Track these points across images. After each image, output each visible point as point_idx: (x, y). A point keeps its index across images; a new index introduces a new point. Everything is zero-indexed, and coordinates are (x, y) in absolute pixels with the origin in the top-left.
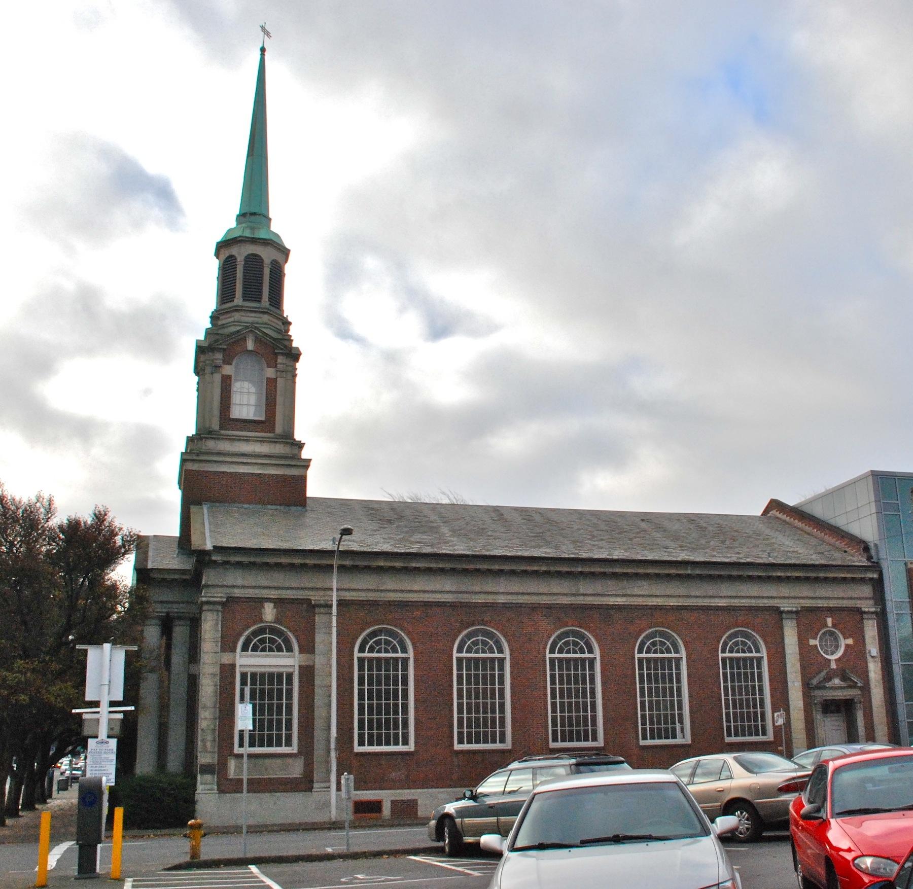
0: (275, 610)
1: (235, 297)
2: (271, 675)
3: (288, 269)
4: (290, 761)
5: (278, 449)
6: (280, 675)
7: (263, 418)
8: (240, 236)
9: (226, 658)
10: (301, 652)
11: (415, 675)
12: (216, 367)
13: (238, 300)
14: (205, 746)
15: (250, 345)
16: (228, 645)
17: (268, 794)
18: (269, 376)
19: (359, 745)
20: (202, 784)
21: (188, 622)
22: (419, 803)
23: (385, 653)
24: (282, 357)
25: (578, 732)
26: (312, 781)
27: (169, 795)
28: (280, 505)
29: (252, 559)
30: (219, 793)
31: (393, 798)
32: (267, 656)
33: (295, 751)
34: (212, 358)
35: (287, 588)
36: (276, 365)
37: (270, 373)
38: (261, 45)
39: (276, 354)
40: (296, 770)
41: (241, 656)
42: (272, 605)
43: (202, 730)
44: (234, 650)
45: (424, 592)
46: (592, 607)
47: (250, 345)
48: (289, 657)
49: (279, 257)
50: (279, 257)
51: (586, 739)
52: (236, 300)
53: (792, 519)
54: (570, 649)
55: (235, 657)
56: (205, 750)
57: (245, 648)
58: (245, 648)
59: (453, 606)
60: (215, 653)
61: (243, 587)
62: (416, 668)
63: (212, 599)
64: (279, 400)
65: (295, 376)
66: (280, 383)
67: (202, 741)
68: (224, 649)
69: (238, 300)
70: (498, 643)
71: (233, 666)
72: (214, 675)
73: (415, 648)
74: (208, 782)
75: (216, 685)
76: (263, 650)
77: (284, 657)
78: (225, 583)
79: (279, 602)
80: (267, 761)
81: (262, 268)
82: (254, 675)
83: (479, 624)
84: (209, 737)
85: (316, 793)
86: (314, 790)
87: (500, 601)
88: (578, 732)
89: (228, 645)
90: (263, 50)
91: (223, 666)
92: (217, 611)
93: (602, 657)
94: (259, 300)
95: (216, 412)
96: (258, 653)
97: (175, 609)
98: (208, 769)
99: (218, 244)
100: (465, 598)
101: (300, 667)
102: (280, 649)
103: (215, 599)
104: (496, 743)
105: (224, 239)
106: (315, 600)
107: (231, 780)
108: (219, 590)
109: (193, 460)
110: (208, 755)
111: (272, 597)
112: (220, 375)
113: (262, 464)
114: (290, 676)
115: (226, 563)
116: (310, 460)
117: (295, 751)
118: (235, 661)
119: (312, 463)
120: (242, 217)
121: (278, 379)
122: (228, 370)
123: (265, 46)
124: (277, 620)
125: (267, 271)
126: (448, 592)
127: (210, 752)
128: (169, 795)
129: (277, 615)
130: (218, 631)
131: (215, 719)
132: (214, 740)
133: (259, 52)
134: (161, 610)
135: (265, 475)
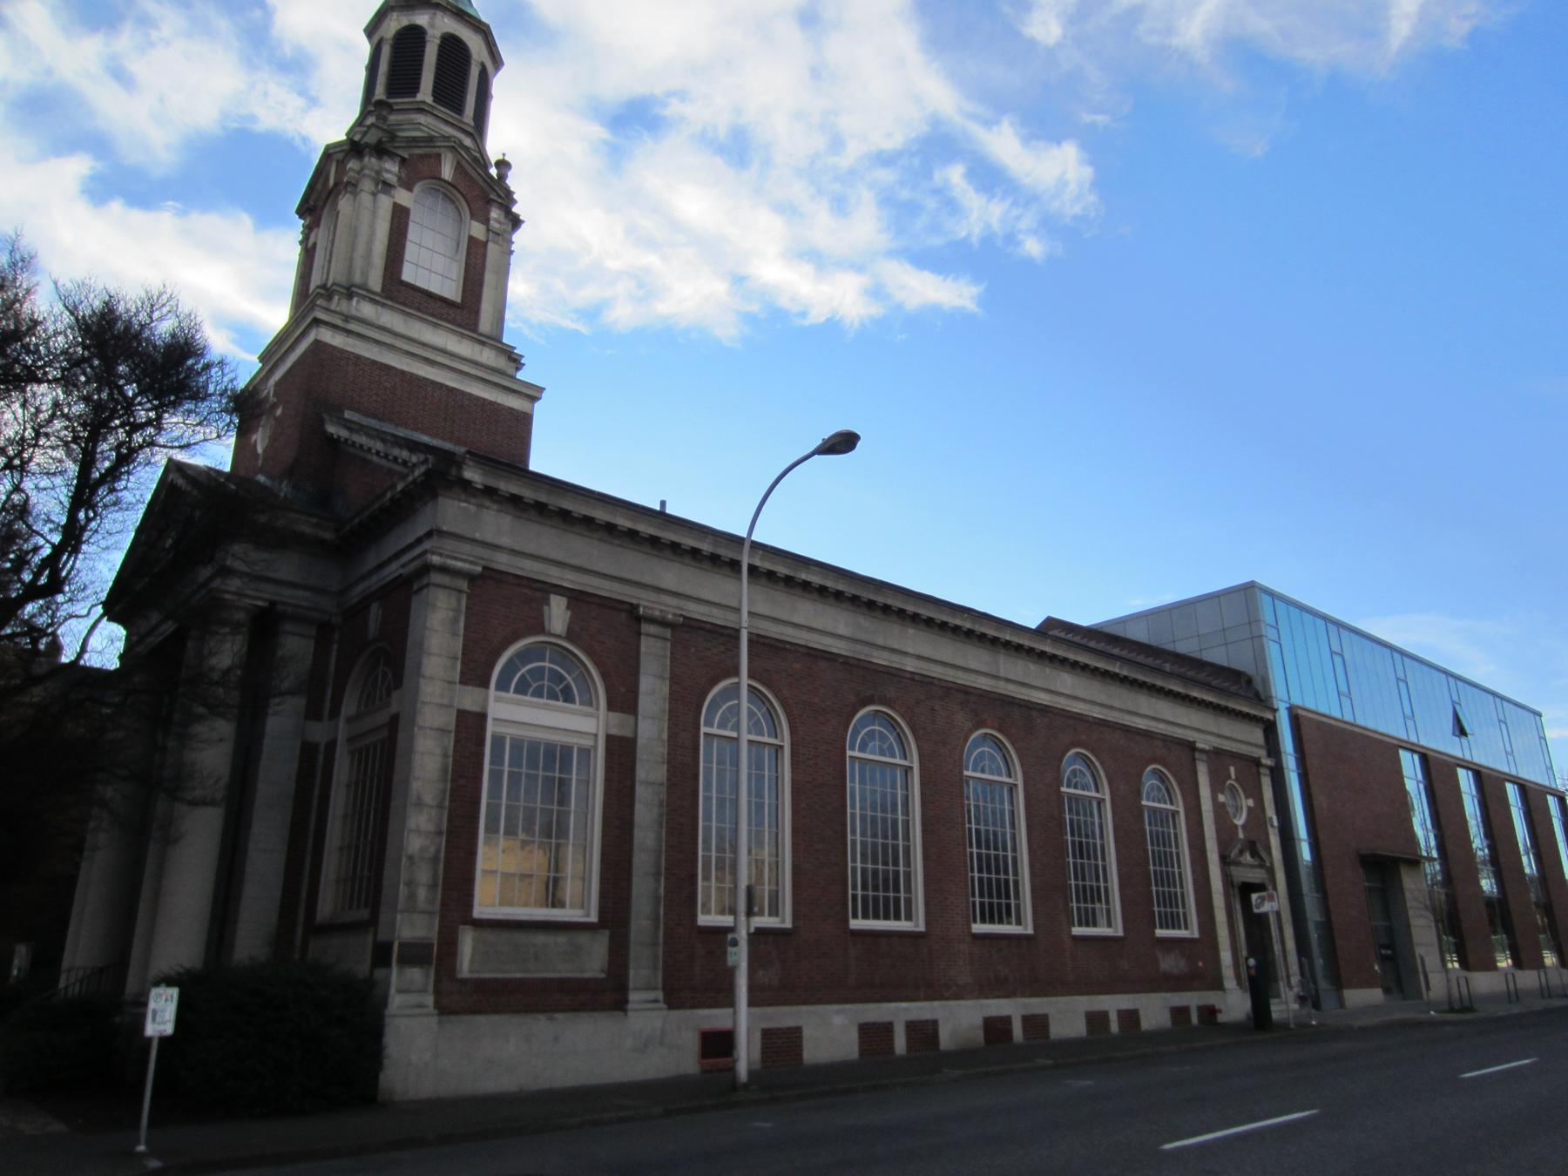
2: (550, 749)
4: (583, 938)
5: (487, 356)
6: (566, 750)
9: (468, 699)
10: (612, 706)
13: (425, 93)
14: (412, 897)
16: (475, 672)
17: (542, 1018)
20: (400, 991)
21: (313, 632)
24: (498, 212)
31: (765, 1026)
32: (546, 707)
33: (594, 918)
35: (699, 601)
37: (477, 230)
39: (489, 202)
40: (593, 960)
41: (497, 700)
43: (410, 858)
44: (484, 683)
47: (447, 172)
52: (420, 97)
53: (1085, 640)
55: (486, 700)
57: (503, 685)
60: (450, 682)
67: (409, 884)
68: (466, 679)
69: (425, 93)
71: (482, 717)
72: (443, 731)
73: (793, 732)
75: (445, 756)
76: (538, 693)
77: (573, 712)
79: (577, 598)
80: (541, 938)
82: (517, 744)
84: (423, 876)
87: (909, 669)
89: (475, 672)
91: (462, 715)
92: (460, 591)
95: (378, 261)
96: (528, 698)
98: (415, 955)
100: (864, 653)
102: (568, 697)
103: (459, 564)
106: (645, 607)
107: (464, 982)
108: (466, 548)
111: (564, 584)
115: (489, 492)
116: (542, 390)
117: (594, 918)
119: (544, 395)
121: (491, 246)
122: (403, 197)
124: (571, 635)
125: (474, 72)
127: (423, 912)
130: (458, 635)
131: (439, 833)
134: (260, 597)
135: (462, 393)
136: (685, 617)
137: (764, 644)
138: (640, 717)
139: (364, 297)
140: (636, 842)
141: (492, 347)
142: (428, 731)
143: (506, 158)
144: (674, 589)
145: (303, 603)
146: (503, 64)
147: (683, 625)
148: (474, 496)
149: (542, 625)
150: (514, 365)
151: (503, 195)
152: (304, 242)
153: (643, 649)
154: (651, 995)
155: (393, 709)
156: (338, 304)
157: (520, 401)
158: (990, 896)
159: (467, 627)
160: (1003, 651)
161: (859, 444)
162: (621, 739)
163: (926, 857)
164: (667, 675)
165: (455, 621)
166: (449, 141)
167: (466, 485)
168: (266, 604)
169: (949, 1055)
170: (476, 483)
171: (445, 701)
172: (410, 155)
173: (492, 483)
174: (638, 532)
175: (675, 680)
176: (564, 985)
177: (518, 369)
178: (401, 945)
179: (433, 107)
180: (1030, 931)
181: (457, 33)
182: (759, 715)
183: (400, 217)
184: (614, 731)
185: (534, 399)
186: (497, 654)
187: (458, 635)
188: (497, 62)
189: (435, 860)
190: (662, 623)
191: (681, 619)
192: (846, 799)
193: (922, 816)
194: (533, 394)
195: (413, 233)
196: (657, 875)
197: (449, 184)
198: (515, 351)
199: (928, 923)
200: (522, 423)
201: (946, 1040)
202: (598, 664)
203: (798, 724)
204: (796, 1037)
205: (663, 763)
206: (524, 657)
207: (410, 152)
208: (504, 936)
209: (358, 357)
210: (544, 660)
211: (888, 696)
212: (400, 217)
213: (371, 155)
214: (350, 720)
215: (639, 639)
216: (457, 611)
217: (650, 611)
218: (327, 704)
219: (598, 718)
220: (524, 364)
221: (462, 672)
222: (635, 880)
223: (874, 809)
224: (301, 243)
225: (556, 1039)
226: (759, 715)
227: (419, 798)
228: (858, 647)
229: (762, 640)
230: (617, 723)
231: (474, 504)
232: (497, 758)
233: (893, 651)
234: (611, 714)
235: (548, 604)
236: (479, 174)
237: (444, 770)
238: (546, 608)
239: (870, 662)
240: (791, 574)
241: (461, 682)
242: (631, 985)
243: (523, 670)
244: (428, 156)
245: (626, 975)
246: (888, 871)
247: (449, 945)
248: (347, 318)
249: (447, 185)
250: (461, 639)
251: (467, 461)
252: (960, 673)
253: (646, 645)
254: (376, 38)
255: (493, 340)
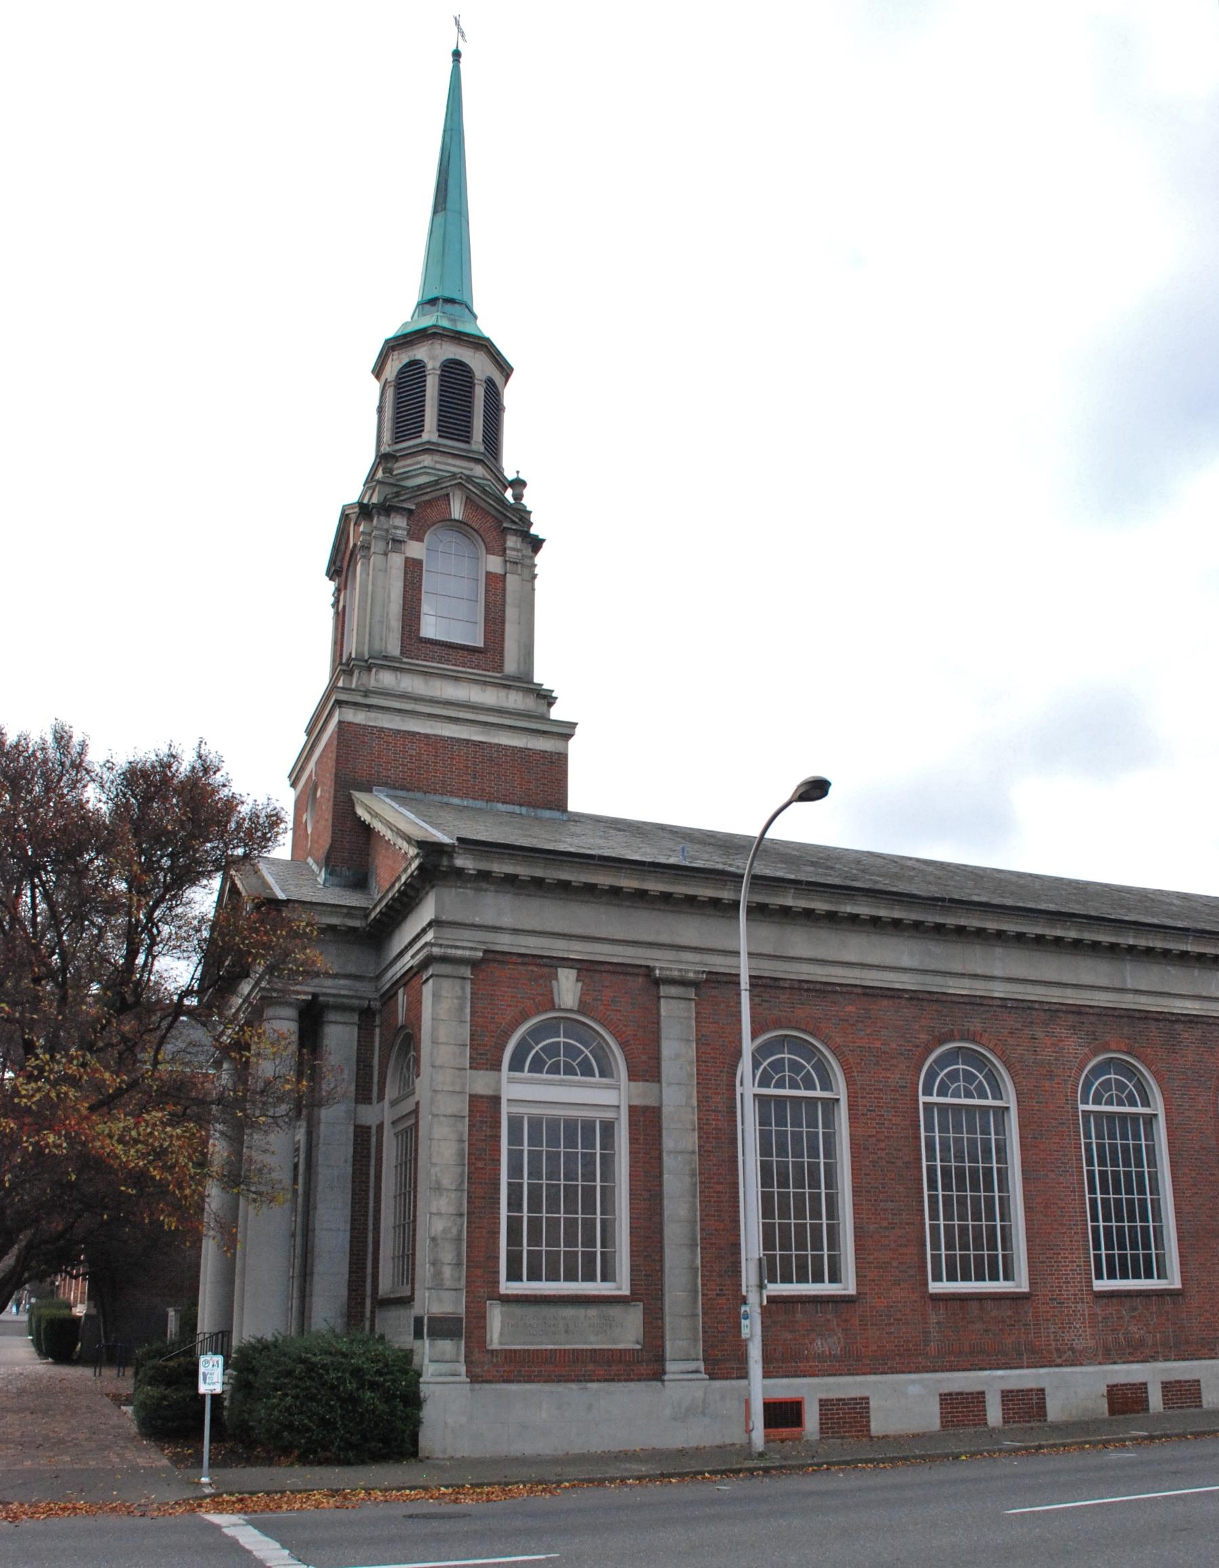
0: (580, 984)
1: (423, 431)
2: (571, 1124)
3: (511, 395)
4: (615, 1311)
5: (514, 700)
6: (588, 1126)
7: (480, 643)
8: (435, 326)
9: (481, 1083)
10: (633, 1076)
11: (852, 1137)
12: (394, 540)
13: (430, 432)
14: (438, 1275)
15: (457, 510)
18: (491, 569)
19: (509, 1279)
21: (356, 1018)
22: (872, 1404)
23: (790, 1088)
24: (514, 538)
25: (802, 1261)
26: (660, 1359)
27: (373, 1386)
28: (521, 805)
29: (539, 873)
30: (471, 1382)
31: (824, 1396)
32: (562, 1083)
33: (626, 1291)
34: (386, 527)
36: (505, 550)
37: (494, 564)
38: (455, 48)
39: (504, 531)
42: (573, 974)
43: (434, 1239)
44: (497, 1067)
45: (863, 966)
46: (1146, 1016)
47: (457, 510)
48: (608, 1087)
49: (497, 378)
50: (497, 378)
51: (818, 1278)
52: (425, 437)
54: (1112, 1095)
55: (499, 1082)
56: (438, 1285)
57: (516, 1065)
58: (516, 1065)
59: (915, 997)
61: (515, 931)
62: (853, 1118)
63: (451, 951)
64: (511, 613)
65: (534, 577)
66: (512, 582)
69: (430, 432)
70: (992, 1078)
71: (496, 1100)
73: (850, 1082)
74: (447, 1357)
75: (461, 1141)
76: (554, 1070)
78: (477, 919)
79: (586, 968)
80: (569, 1312)
81: (471, 386)
82: (535, 1123)
83: (962, 1039)
84: (447, 1255)
85: (673, 1384)
86: (666, 1377)
87: (996, 995)
88: (802, 1261)
90: (457, 55)
91: (474, 1099)
93: (1168, 1112)
94: (467, 439)
95: (396, 624)
96: (544, 1076)
97: (328, 987)
98: (442, 1328)
99: (387, 341)
101: (632, 1109)
102: (587, 1071)
103: (459, 952)
104: (823, 1281)
105: (399, 334)
106: (661, 969)
108: (467, 934)
109: (355, 704)
110: (447, 1295)
112: (403, 557)
113: (486, 724)
114: (608, 1128)
116: (573, 725)
117: (626, 1291)
118: (499, 1089)
119: (578, 730)
120: (428, 303)
121: (508, 575)
122: (415, 549)
123: (460, 49)
124: (583, 1008)
125: (479, 392)
126: (905, 970)
128: (373, 1386)
129: (583, 994)
132: (459, 1264)
133: (451, 59)
136: (710, 973)
137: (808, 990)
138: (664, 1085)
139: (382, 667)
140: (666, 1213)
141: (518, 689)
142: (442, 1119)
143: (522, 476)
144: (694, 944)
145: (343, 992)
146: (512, 369)
147: (707, 980)
148: (469, 881)
149: (552, 1001)
150: (544, 702)
151: (517, 520)
152: (336, 604)
153: (663, 1013)
154: (692, 1366)
155: (417, 1100)
156: (359, 679)
157: (552, 741)
158: (1122, 1246)
159: (473, 1013)
160: (1129, 958)
161: (831, 790)
162: (646, 1109)
163: (1028, 1209)
164: (693, 1037)
165: (461, 1009)
166: (456, 479)
167: (460, 873)
168: (310, 997)
169: (1057, 1428)
170: (469, 869)
171: (458, 1089)
172: (416, 504)
173: (485, 866)
174: (647, 891)
175: (701, 1042)
176: (595, 1356)
177: (550, 704)
178: (429, 1319)
179: (439, 445)
180: (1177, 1285)
181: (458, 357)
182: (809, 1067)
183: (413, 569)
184: (636, 1102)
185: (568, 736)
186: (507, 1036)
187: (465, 1022)
188: (506, 370)
189: (458, 1239)
190: (683, 983)
191: (705, 976)
192: (920, 1150)
193: (1168, 1128)
194: (566, 731)
195: (428, 582)
196: (693, 1245)
197: (461, 522)
198: (544, 687)
199: (1032, 1283)
200: (557, 765)
201: (1055, 1410)
202: (616, 1035)
203: (855, 1074)
204: (945, 1408)
205: (694, 1130)
206: (537, 1033)
207: (416, 501)
208: (531, 1311)
209: (381, 729)
210: (559, 1037)
211: (972, 1028)
212: (413, 569)
213: (379, 514)
214: (394, 1103)
215: (659, 1001)
216: (462, 998)
217: (668, 973)
218: (375, 1088)
219: (619, 1089)
220: (556, 698)
221: (471, 1058)
222: (668, 1252)
223: (959, 1157)
224: (333, 606)
225: (590, 1408)
226: (809, 1067)
227: (438, 1182)
228: (929, 979)
229: (806, 986)
230: (640, 1094)
231: (471, 888)
232: (515, 1138)
233: (975, 976)
234: (632, 1083)
235: (557, 979)
236: (490, 504)
237: (461, 1154)
238: (554, 982)
239: (945, 993)
240: (832, 908)
241: (471, 1068)
242: (668, 1355)
243: (537, 1048)
244: (437, 499)
245: (662, 1347)
246: (1121, 1199)
247: (477, 1319)
248: (366, 693)
249: (458, 524)
250: (469, 1024)
251: (457, 849)
252: (1069, 992)
253: (667, 1008)
254: (383, 380)
255: (524, 682)
